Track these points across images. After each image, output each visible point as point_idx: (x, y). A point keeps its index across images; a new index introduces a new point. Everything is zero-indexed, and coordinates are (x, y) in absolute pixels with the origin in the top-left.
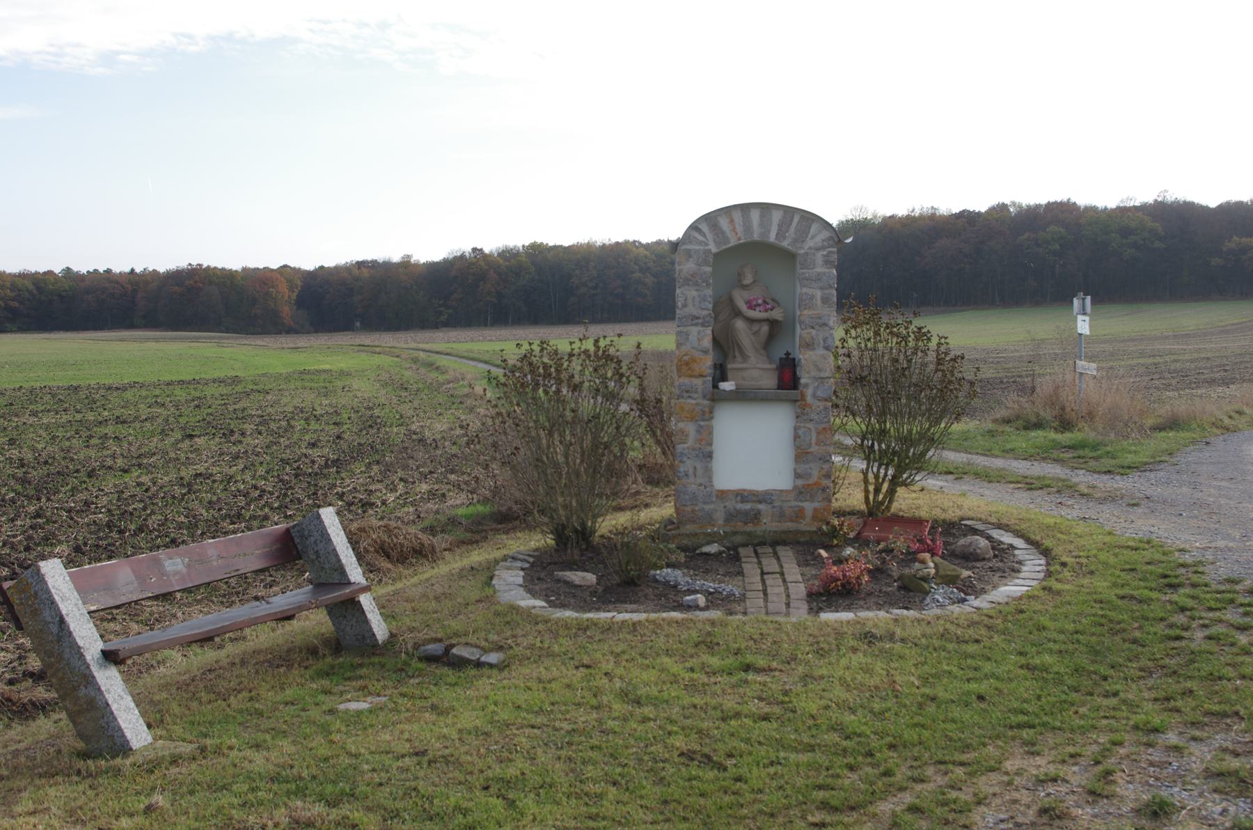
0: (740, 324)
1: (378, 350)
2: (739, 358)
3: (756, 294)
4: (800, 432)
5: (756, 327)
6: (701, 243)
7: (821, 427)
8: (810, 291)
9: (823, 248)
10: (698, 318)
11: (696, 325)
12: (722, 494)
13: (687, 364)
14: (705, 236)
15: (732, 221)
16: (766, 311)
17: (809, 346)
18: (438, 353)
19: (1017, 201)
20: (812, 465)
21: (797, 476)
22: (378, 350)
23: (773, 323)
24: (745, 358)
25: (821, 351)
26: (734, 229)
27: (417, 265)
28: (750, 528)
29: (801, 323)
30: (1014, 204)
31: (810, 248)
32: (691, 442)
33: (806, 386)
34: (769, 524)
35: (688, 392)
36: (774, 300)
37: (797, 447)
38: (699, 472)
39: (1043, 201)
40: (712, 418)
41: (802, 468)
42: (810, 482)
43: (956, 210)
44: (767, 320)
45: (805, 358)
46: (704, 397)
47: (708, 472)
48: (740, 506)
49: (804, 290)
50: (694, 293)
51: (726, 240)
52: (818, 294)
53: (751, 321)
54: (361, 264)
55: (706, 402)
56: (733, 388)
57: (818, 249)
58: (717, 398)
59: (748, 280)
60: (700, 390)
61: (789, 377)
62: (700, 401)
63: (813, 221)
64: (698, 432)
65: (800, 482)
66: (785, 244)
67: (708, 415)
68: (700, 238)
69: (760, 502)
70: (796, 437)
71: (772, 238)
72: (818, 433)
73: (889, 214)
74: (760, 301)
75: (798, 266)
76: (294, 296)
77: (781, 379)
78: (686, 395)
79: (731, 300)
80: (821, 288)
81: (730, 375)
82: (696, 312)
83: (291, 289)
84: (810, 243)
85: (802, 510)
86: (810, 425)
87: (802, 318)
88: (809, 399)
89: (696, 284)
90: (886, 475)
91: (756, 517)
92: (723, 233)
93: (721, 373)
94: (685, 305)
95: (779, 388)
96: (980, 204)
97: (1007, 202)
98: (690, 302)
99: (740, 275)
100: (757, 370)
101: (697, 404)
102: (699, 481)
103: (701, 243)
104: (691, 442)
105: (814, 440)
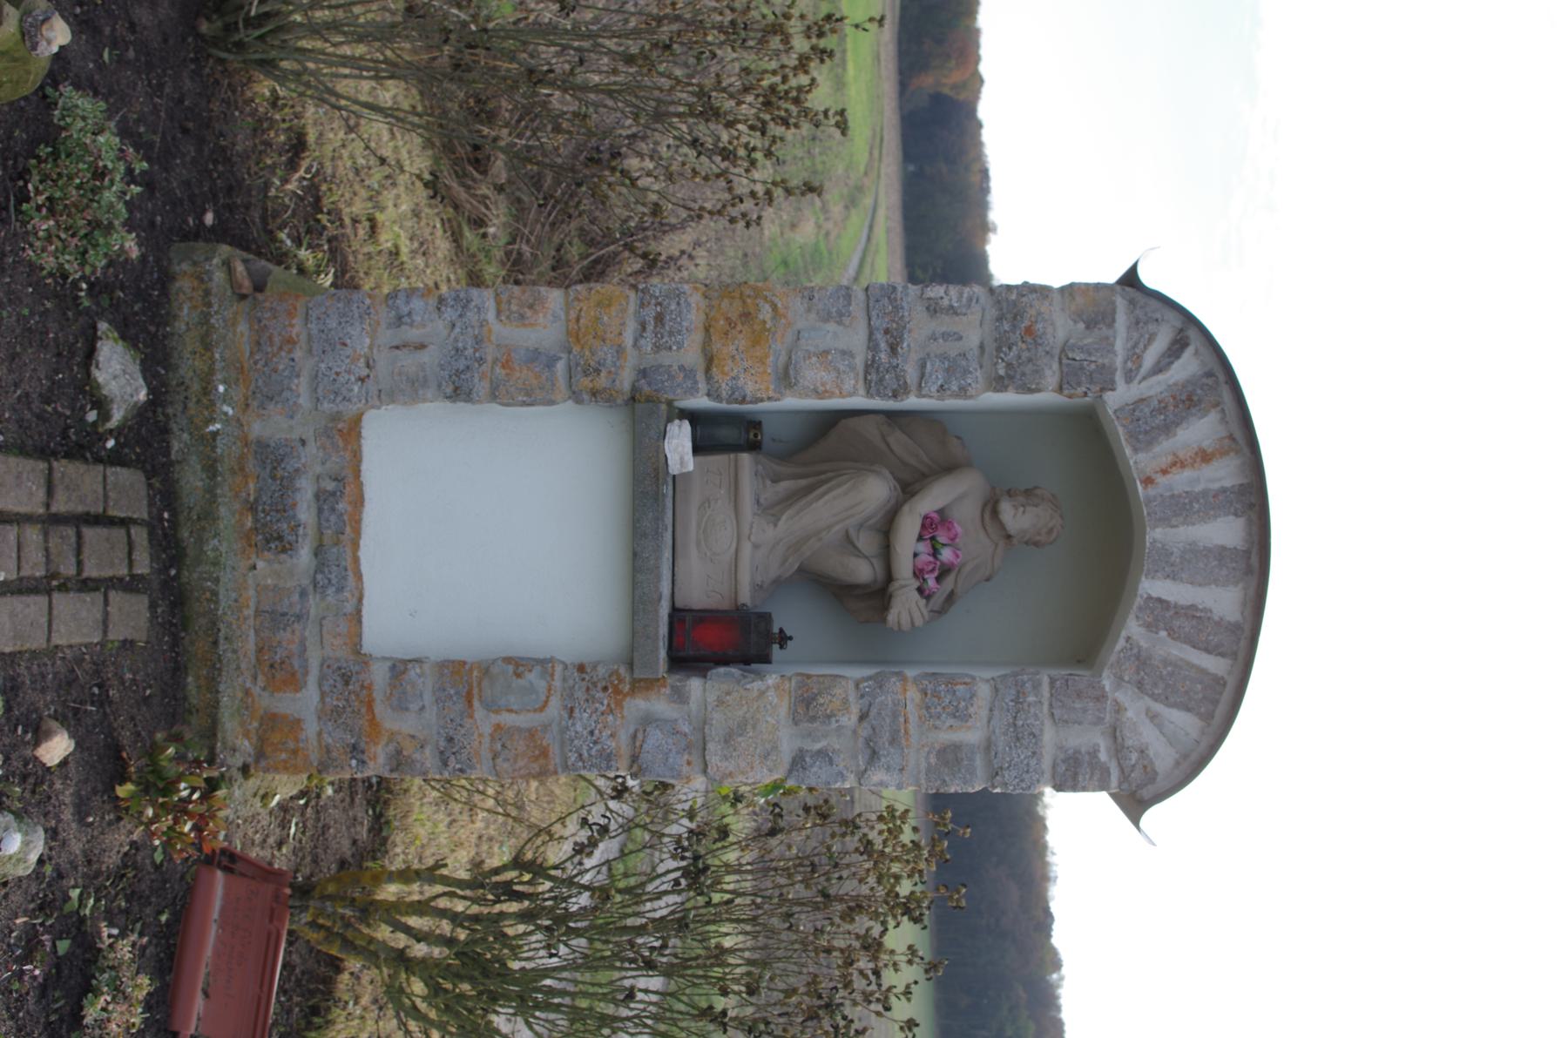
0: (875, 491)
1: (876, 153)
2: (773, 491)
3: (970, 544)
4: (533, 677)
5: (868, 542)
6: (1135, 356)
7: (551, 740)
8: (980, 707)
9: (1119, 749)
10: (893, 349)
11: (872, 345)
12: (348, 433)
13: (746, 316)
14: (1158, 369)
15: (1205, 457)
16: (918, 573)
17: (806, 706)
18: (871, 227)
19: (1065, 983)
20: (431, 714)
21: (399, 668)
22: (876, 153)
23: (879, 595)
24: (771, 511)
25: (788, 745)
26: (1178, 463)
27: (984, 241)
28: (228, 513)
29: (880, 681)
30: (1062, 978)
31: (1119, 709)
32: (503, 332)
33: (680, 697)
34: (241, 581)
35: (660, 323)
36: (951, 598)
37: (485, 669)
38: (408, 361)
39: (1065, 1015)
40: (576, 397)
41: (423, 683)
42: (379, 708)
43: (1054, 907)
44: (889, 577)
45: (766, 694)
46: (643, 373)
47: (409, 390)
48: (306, 490)
49: (984, 691)
50: (973, 339)
51: (1144, 439)
52: (971, 735)
53: (886, 527)
54: (985, 173)
55: (626, 380)
56: (674, 468)
57: (1114, 733)
58: (643, 410)
59: (1014, 517)
60: (666, 358)
61: (716, 640)
62: (631, 362)
63: (1207, 717)
64: (534, 355)
65: (379, 676)
66: (1133, 628)
67: (588, 388)
68: (1150, 358)
69: (318, 552)
70: (519, 665)
71: (1152, 587)
72: (531, 734)
73: (1048, 823)
74: (946, 555)
75: (1054, 672)
76: (946, 91)
77: (705, 617)
78: (650, 313)
79: (949, 468)
80: (989, 746)
81: (718, 461)
82: (913, 342)
83: (955, 87)
84: (1134, 707)
85: (294, 682)
86: (555, 708)
87: (894, 684)
88: (638, 705)
89: (1002, 343)
90: (419, 936)
91: (273, 537)
92: (1168, 429)
93: (720, 434)
94: (933, 309)
95: (677, 614)
96: (1060, 937)
97: (1064, 971)
98: (945, 324)
99: (1029, 495)
100: (733, 543)
101: (620, 351)
102: (383, 360)
103: (1135, 356)
104: (503, 332)
105: (507, 719)
